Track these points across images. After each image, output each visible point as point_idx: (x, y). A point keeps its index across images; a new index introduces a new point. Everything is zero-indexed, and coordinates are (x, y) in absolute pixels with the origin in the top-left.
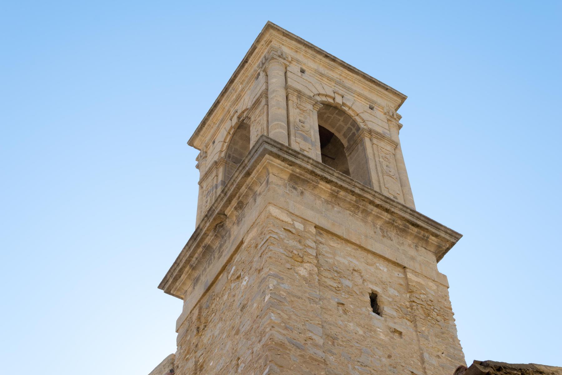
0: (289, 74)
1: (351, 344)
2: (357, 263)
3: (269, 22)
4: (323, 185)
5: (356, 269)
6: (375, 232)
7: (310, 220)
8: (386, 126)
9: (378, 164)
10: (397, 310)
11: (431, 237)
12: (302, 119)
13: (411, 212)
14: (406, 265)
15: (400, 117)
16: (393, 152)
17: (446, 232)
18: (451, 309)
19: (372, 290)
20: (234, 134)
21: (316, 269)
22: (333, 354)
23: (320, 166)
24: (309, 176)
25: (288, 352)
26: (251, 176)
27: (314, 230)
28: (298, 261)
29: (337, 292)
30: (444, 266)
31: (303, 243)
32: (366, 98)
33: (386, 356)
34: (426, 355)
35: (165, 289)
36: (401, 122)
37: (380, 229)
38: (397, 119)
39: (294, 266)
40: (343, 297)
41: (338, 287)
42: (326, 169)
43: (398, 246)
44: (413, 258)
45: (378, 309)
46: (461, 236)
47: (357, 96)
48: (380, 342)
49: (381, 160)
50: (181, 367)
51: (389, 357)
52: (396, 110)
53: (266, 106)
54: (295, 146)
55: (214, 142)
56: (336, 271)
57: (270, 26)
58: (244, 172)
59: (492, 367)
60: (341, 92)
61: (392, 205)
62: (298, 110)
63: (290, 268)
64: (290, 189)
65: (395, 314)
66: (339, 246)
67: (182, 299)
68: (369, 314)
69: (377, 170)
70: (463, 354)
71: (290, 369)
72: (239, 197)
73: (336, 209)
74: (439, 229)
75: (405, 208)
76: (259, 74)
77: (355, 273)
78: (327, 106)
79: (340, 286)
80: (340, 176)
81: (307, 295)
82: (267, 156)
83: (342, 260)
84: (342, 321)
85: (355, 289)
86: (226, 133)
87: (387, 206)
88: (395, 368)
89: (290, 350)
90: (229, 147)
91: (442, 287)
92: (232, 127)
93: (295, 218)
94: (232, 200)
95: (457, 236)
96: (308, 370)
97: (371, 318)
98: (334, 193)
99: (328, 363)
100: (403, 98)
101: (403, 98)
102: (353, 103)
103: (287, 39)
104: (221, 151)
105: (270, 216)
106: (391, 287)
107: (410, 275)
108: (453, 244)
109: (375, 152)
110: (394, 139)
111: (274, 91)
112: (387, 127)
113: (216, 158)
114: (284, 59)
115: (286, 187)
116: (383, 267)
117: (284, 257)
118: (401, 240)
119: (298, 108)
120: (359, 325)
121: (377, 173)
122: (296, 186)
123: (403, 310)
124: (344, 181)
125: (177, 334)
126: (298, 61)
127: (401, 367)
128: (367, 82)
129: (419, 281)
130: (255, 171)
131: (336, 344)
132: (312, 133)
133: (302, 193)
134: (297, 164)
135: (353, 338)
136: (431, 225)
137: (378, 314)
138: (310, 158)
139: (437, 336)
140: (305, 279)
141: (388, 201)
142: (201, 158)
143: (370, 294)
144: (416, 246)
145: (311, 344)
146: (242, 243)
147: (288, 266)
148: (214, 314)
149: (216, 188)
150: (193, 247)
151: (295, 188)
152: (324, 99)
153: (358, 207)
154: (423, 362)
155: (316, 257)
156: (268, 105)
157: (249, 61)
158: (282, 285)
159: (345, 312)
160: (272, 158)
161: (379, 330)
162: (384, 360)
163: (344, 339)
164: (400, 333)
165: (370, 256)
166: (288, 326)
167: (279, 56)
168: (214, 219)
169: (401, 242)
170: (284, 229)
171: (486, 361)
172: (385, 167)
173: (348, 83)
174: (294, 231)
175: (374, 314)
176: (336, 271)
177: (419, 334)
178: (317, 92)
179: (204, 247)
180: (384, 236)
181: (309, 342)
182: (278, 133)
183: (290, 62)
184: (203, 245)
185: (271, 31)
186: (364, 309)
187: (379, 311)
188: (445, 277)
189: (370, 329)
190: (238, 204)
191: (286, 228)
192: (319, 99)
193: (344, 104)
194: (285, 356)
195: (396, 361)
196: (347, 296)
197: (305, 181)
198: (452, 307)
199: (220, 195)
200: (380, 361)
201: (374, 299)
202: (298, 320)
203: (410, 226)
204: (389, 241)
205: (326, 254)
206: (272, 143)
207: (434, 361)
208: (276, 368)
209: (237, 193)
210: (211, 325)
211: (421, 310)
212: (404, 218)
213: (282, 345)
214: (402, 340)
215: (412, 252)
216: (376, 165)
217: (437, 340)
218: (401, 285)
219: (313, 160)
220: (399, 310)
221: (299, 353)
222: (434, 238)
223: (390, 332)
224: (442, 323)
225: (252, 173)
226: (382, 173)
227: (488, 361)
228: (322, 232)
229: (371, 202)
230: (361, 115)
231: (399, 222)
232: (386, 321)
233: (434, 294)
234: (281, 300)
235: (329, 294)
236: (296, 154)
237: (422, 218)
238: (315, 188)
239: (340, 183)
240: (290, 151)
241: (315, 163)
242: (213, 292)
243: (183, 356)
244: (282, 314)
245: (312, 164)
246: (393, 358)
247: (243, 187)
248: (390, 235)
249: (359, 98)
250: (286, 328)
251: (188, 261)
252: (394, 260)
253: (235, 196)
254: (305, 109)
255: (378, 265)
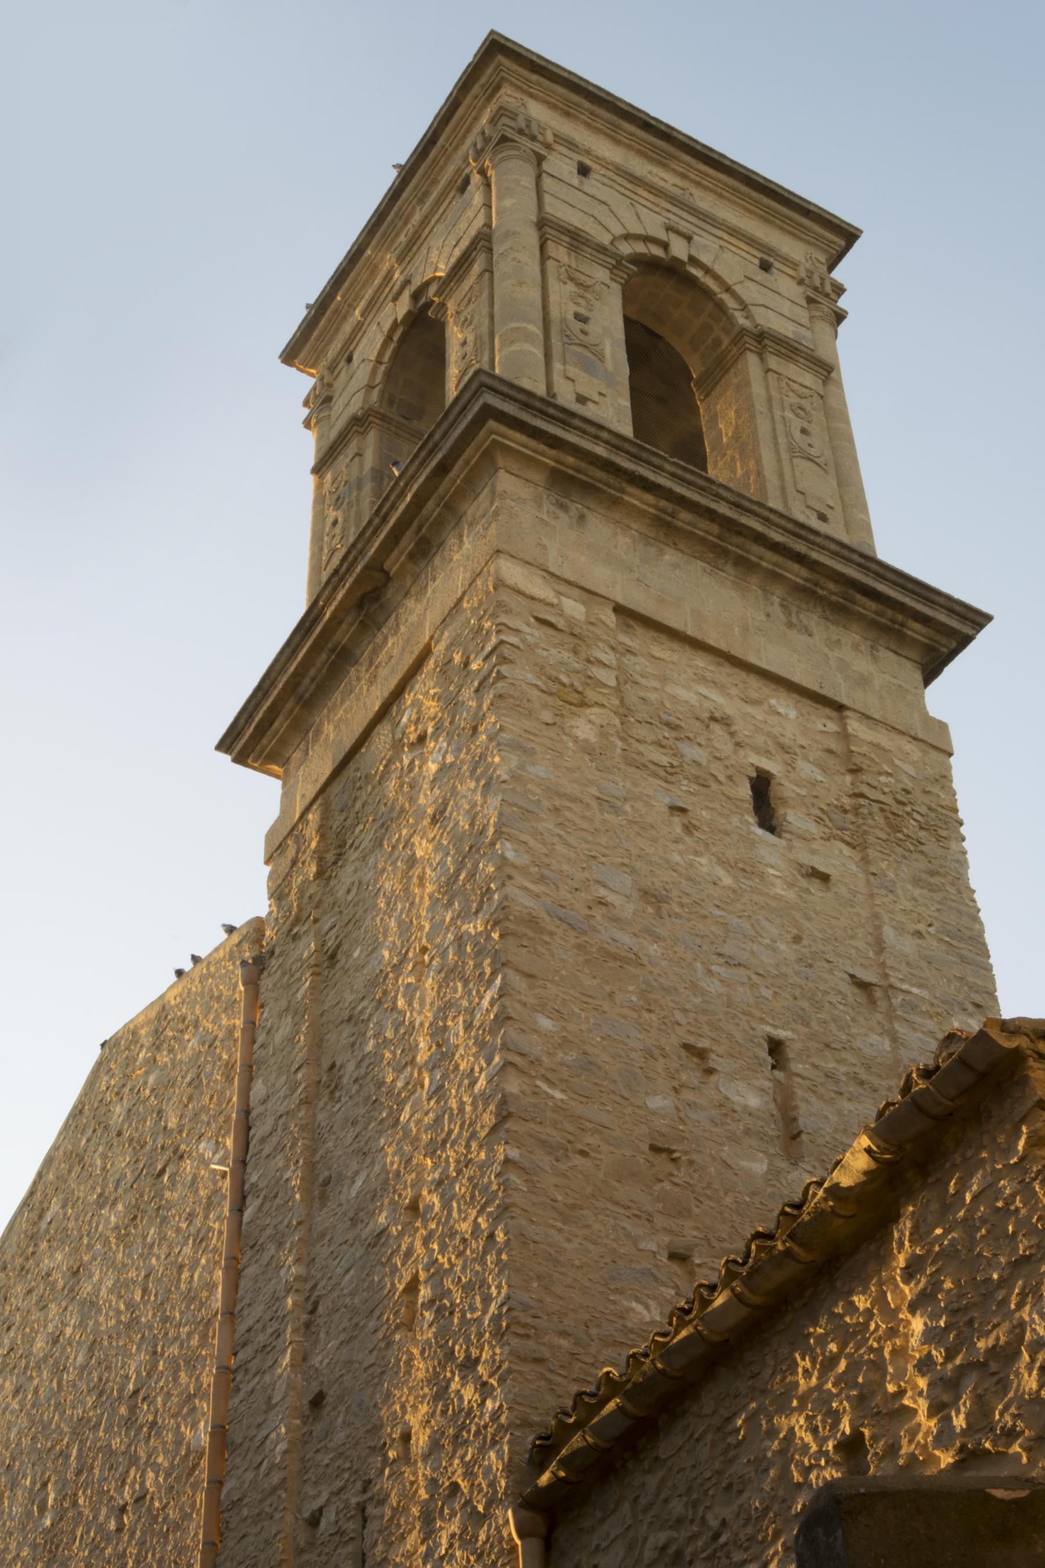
0: (547, 182)
1: (704, 912)
2: (721, 700)
3: (492, 32)
4: (635, 497)
5: (717, 715)
6: (768, 615)
7: (603, 591)
8: (803, 315)
9: (780, 427)
10: (819, 820)
11: (911, 623)
12: (582, 311)
13: (862, 561)
14: (844, 701)
15: (840, 290)
16: (820, 389)
17: (951, 611)
18: (956, 811)
19: (758, 770)
20: (402, 340)
21: (617, 721)
22: (657, 938)
23: (626, 446)
24: (600, 474)
25: (547, 938)
26: (452, 474)
27: (610, 618)
28: (571, 704)
29: (670, 778)
30: (945, 697)
31: (583, 655)
32: (751, 241)
33: (789, 937)
34: (889, 933)
35: (236, 751)
36: (843, 303)
37: (782, 605)
38: (833, 296)
39: (562, 716)
40: (682, 792)
41: (672, 766)
42: (644, 455)
43: (826, 650)
44: (863, 681)
45: (772, 816)
46: (989, 618)
47: (726, 236)
48: (774, 903)
49: (788, 414)
50: (281, 954)
51: (797, 939)
52: (831, 267)
53: (487, 275)
54: (566, 397)
55: (350, 360)
56: (668, 724)
57: (496, 47)
58: (434, 463)
59: (1027, 1035)
60: (684, 227)
61: (813, 543)
62: (571, 287)
63: (550, 721)
64: (552, 508)
65: (813, 828)
66: (675, 657)
67: (278, 777)
68: (749, 832)
69: (776, 445)
70: (981, 924)
71: (553, 982)
72: (420, 528)
73: (667, 557)
74: (933, 602)
75: (844, 551)
76: (467, 181)
77: (716, 727)
78: (648, 265)
79: (675, 763)
80: (679, 472)
81: (594, 791)
82: (492, 424)
83: (684, 694)
84: (680, 853)
85: (716, 768)
86: (380, 340)
87: (800, 547)
88: (811, 966)
89: (551, 934)
90: (389, 375)
91: (933, 754)
92: (395, 325)
93: (563, 588)
94: (403, 534)
95: (979, 619)
96: (595, 982)
97: (753, 844)
98: (663, 516)
99: (645, 960)
100: (849, 236)
101: (849, 236)
102: (717, 257)
103: (543, 80)
104: (370, 387)
105: (500, 584)
106: (805, 758)
107: (854, 725)
108: (965, 641)
109: (773, 393)
110: (822, 353)
111: (507, 235)
112: (805, 321)
113: (355, 406)
114: (533, 138)
115: (540, 506)
116: (786, 706)
117: (536, 692)
118: (835, 632)
119: (571, 279)
120: (723, 862)
121: (777, 452)
122: (566, 501)
123: (834, 816)
124: (690, 483)
125: (268, 869)
126: (571, 145)
127: (826, 965)
128: (754, 194)
129: (876, 741)
130: (460, 462)
131: (664, 912)
132: (608, 350)
133: (582, 518)
134: (568, 443)
135: (709, 896)
136: (913, 592)
137: (772, 830)
138: (601, 427)
139: (917, 882)
140: (586, 748)
141: (803, 532)
142: (320, 402)
143: (751, 779)
144: (872, 647)
145: (603, 915)
146: (426, 653)
147: (547, 716)
148: (361, 827)
149: (360, 487)
150: (304, 650)
151: (563, 507)
152: (640, 248)
153: (725, 553)
154: (880, 946)
155: (618, 690)
156: (492, 272)
157: (441, 141)
158: (531, 769)
159: (689, 829)
160: (503, 429)
161: (771, 871)
162: (783, 947)
163: (685, 900)
164: (825, 878)
165: (753, 681)
166: (546, 872)
167: (521, 132)
168: (357, 582)
169: (835, 638)
170: (537, 619)
171: (1013, 1020)
172: (797, 435)
173: (704, 201)
174: (561, 623)
175: (760, 832)
176: (668, 724)
177: (872, 878)
178: (619, 231)
179: (333, 651)
180: (790, 625)
181: (598, 912)
182: (519, 361)
183: (548, 147)
184: (330, 646)
185: (500, 58)
186: (735, 820)
187: (774, 822)
188: (943, 727)
189: (747, 869)
190: (417, 544)
191: (541, 616)
192: (626, 249)
193: (693, 260)
194: (542, 950)
195: (814, 949)
196: (694, 787)
197: (588, 489)
198: (960, 805)
199: (370, 522)
200: (774, 950)
201: (762, 786)
202: (573, 856)
203: (858, 597)
204: (804, 638)
205: (643, 681)
206: (505, 389)
207: (907, 946)
208: (516, 980)
209: (414, 517)
210: (353, 855)
211: (879, 818)
212: (842, 575)
213: (532, 921)
214: (830, 895)
215: (862, 664)
216: (774, 430)
217: (917, 892)
218: (830, 752)
219: (610, 431)
220: (824, 817)
221: (574, 941)
222: (917, 626)
223: (799, 877)
224: (931, 847)
225: (453, 466)
226: (791, 449)
227: (1019, 1019)
228: (631, 622)
229: (760, 539)
230: (738, 289)
231: (831, 586)
232: (790, 848)
233: (913, 773)
234: (530, 808)
235: (651, 786)
236: (567, 417)
237: (889, 575)
238: (614, 503)
239: (679, 489)
240: (551, 411)
241: (614, 440)
242: (357, 770)
243: (285, 929)
244: (532, 842)
245: (607, 442)
246: (805, 942)
247: (431, 504)
248: (805, 622)
249: (733, 240)
250: (542, 879)
251: (292, 686)
252: (815, 688)
253: (409, 525)
254: (590, 282)
255: (773, 702)
